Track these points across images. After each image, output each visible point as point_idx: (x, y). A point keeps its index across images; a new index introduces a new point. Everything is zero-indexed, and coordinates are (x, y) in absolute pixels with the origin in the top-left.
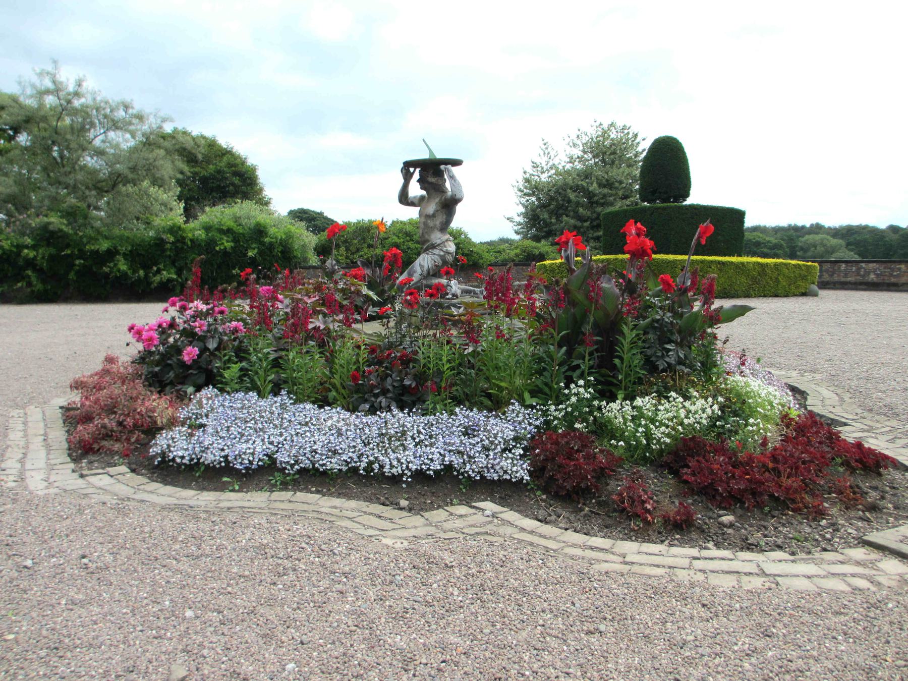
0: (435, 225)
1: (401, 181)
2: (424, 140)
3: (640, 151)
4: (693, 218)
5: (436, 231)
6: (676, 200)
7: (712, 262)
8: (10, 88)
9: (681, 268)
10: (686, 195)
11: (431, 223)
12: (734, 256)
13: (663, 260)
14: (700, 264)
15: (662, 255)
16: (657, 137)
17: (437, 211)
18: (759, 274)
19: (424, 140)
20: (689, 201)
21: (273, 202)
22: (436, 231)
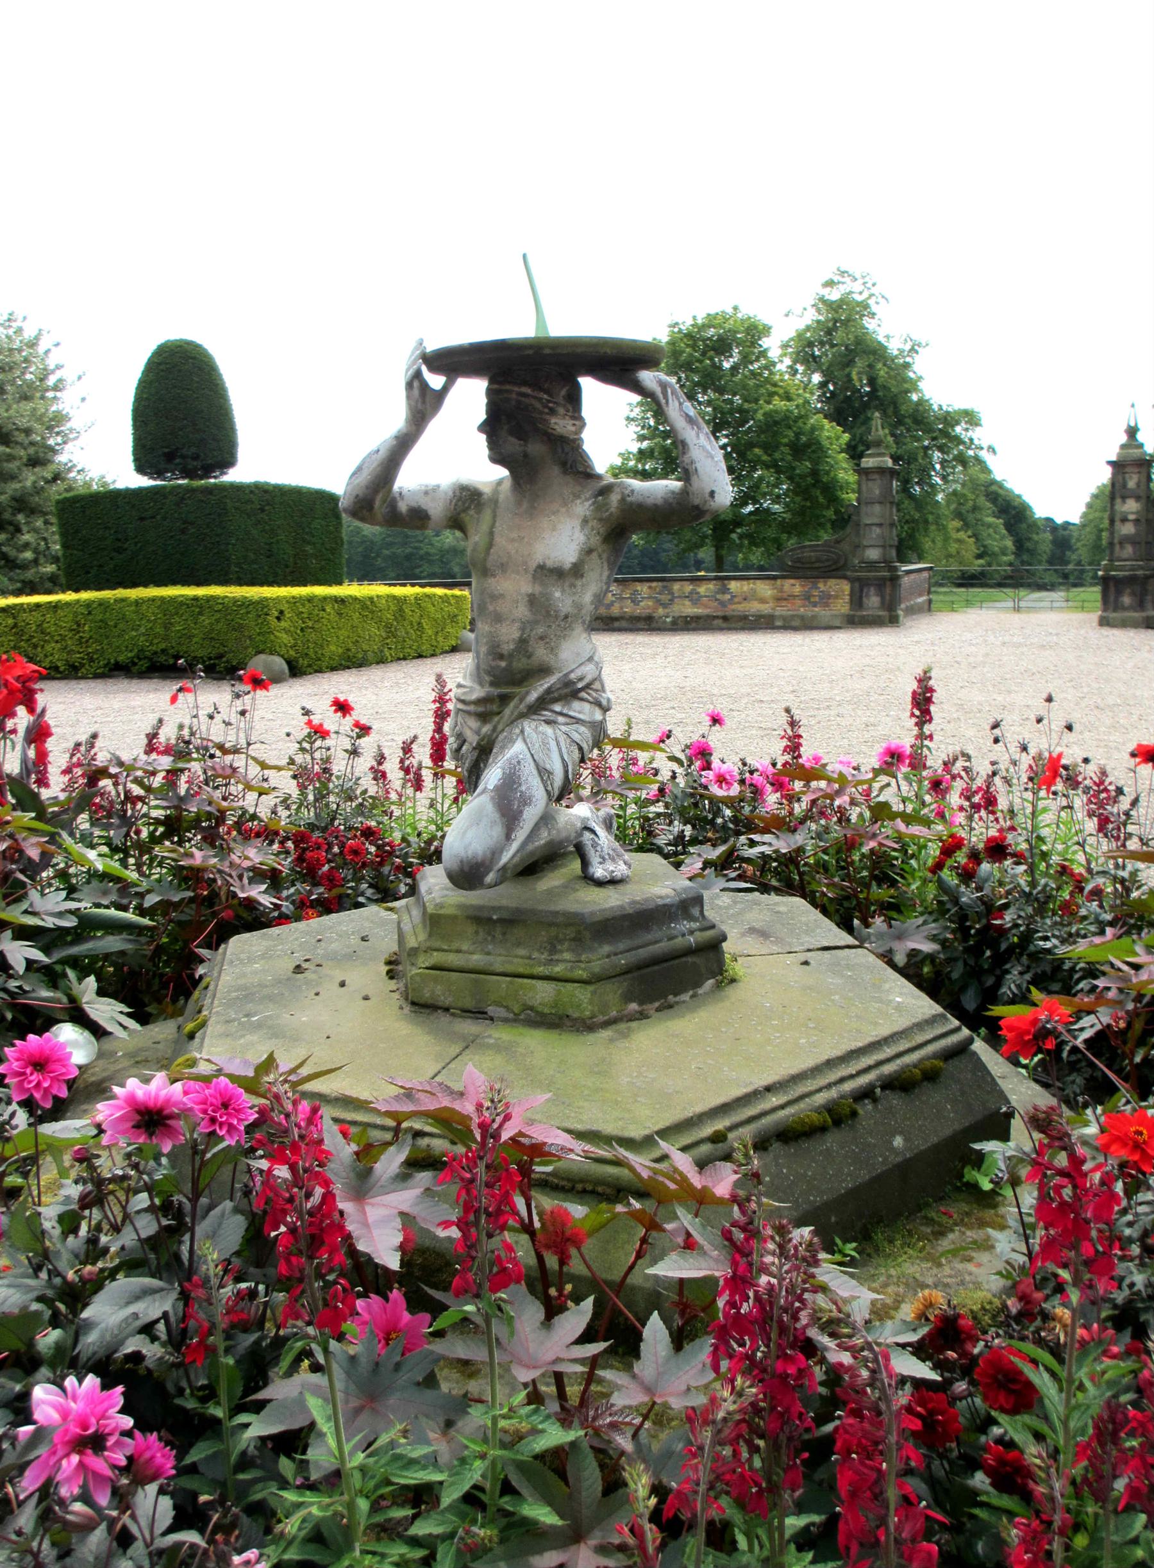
0: (579, 607)
1: (397, 418)
2: (524, 256)
3: (52, 367)
4: (262, 510)
5: (579, 629)
6: (207, 471)
7: (325, 599)
8: (6, 1308)
9: (276, 614)
10: (227, 460)
11: (561, 598)
12: (340, 583)
13: (235, 601)
14: (308, 605)
15: (289, 589)
16: (199, 341)
17: (590, 551)
18: (396, 619)
19: (524, 256)
20: (234, 476)
21: (1095, 623)
22: (579, 629)
